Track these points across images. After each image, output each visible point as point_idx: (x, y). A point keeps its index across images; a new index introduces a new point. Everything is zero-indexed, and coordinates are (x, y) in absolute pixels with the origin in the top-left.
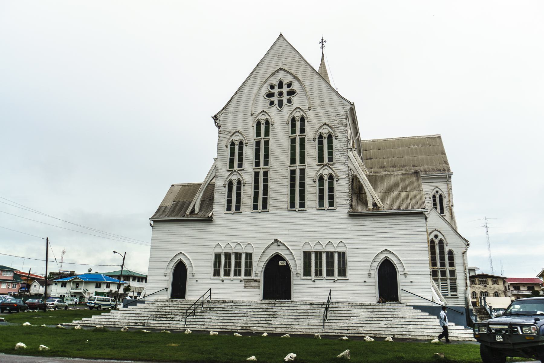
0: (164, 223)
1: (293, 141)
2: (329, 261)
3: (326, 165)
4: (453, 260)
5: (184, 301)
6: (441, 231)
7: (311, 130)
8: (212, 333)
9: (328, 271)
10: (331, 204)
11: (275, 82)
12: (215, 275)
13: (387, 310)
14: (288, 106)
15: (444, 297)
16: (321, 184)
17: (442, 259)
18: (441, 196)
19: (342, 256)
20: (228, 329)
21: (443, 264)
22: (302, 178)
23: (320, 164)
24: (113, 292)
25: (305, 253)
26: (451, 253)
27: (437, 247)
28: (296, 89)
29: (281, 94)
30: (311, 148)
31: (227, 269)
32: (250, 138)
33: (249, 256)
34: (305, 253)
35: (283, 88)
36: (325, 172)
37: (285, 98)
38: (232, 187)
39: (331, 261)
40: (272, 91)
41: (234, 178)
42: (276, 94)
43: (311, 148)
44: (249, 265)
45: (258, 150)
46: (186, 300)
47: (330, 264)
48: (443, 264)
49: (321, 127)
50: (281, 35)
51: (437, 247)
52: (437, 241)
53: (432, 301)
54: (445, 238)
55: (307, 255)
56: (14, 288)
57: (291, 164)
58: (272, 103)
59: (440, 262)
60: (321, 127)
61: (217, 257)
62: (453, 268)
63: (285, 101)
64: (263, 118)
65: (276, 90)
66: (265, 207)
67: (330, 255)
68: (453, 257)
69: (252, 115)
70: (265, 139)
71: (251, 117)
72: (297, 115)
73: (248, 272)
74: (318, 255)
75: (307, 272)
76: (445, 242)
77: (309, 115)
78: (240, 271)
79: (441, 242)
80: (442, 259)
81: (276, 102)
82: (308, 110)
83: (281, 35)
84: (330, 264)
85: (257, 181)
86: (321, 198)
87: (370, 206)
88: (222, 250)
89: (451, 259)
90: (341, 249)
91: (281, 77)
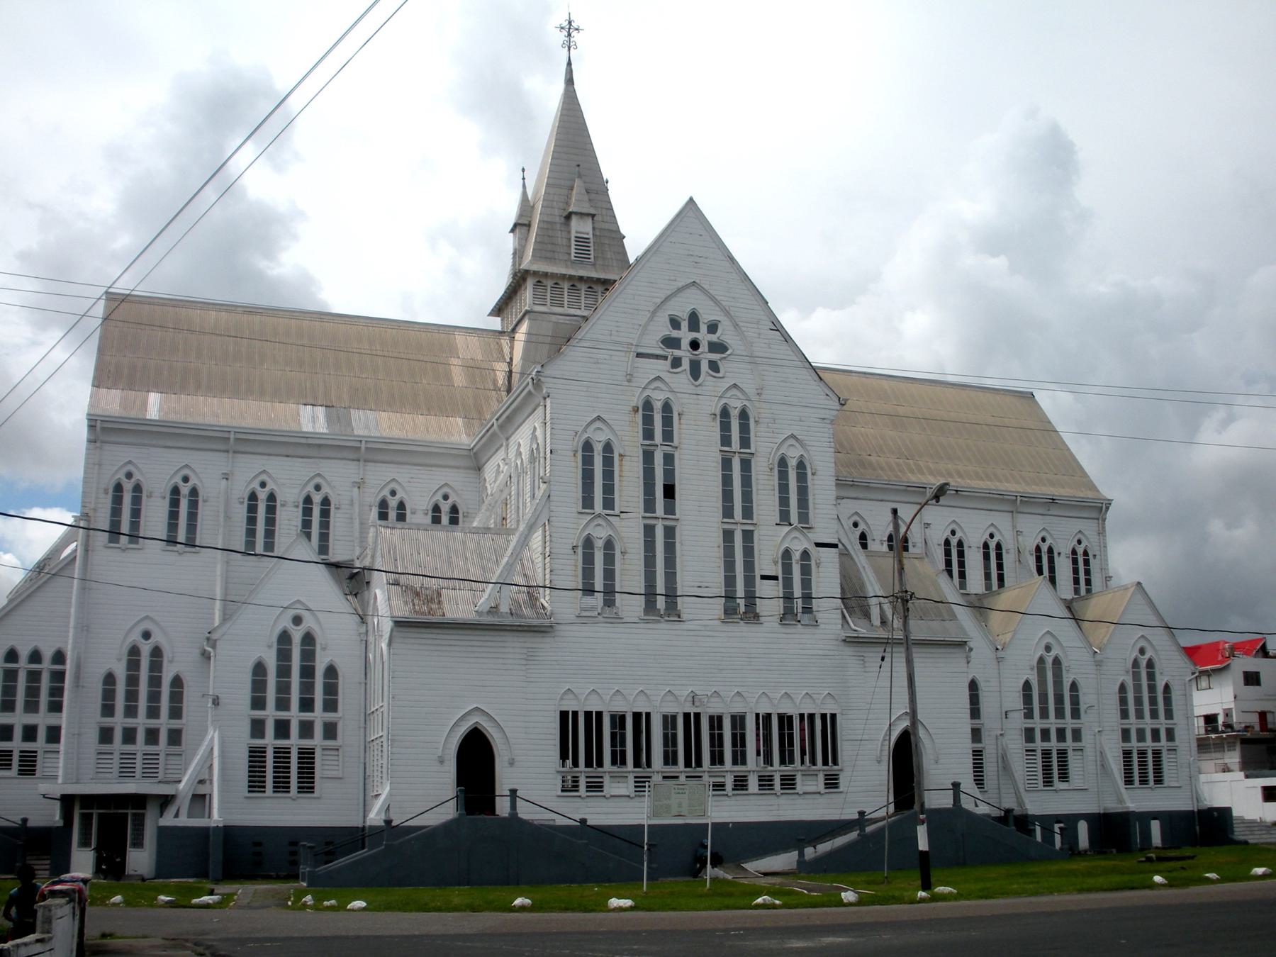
0: (461, 632)
1: (726, 464)
2: (715, 733)
3: (599, 516)
8: (1114, 851)
9: (734, 754)
11: (683, 315)
15: (980, 792)
17: (154, 697)
19: (830, 721)
23: (666, 516)
24: (394, 824)
28: (729, 342)
29: (695, 345)
31: (618, 749)
32: (629, 441)
36: (600, 534)
37: (705, 356)
38: (593, 554)
41: (600, 534)
42: (685, 344)
50: (691, 199)
56: (673, 791)
57: (583, 508)
61: (564, 715)
63: (704, 366)
64: (658, 398)
70: (645, 447)
71: (627, 384)
72: (736, 405)
78: (721, 754)
80: (154, 697)
83: (691, 199)
85: (649, 546)
87: (876, 621)
88: (582, 704)
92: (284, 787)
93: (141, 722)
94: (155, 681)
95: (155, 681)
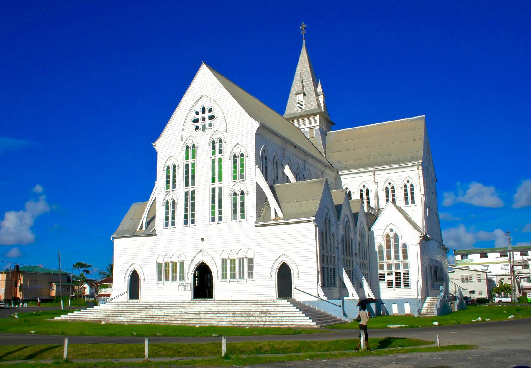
4: (407, 253)
5: (139, 302)
6: (396, 225)
7: (227, 149)
9: (240, 274)
10: (243, 216)
12: (159, 280)
13: (203, 304)
14: (210, 129)
16: (235, 199)
17: (397, 252)
18: (412, 185)
20: (274, 325)
21: (397, 258)
22: (220, 195)
25: (223, 260)
26: (405, 246)
27: (392, 241)
30: (228, 166)
33: (182, 264)
34: (223, 260)
35: (205, 113)
39: (70, 283)
40: (197, 117)
43: (228, 166)
44: (182, 271)
45: (187, 172)
46: (140, 301)
47: (241, 268)
48: (397, 258)
49: (235, 147)
51: (392, 241)
52: (391, 235)
53: (317, 296)
54: (399, 230)
55: (224, 262)
58: (197, 128)
59: (379, 256)
60: (235, 147)
61: (160, 265)
62: (398, 261)
63: (207, 126)
65: (200, 116)
66: (193, 222)
67: (241, 261)
68: (407, 250)
69: (182, 140)
73: (182, 278)
74: (233, 261)
75: (224, 276)
76: (399, 235)
77: (226, 137)
79: (396, 236)
80: (397, 252)
81: (200, 127)
82: (225, 132)
84: (241, 268)
86: (235, 211)
89: (405, 251)
90: (249, 255)
91: (203, 103)
92: (405, 273)
93: (393, 261)
94: (396, 246)
95: (396, 246)
